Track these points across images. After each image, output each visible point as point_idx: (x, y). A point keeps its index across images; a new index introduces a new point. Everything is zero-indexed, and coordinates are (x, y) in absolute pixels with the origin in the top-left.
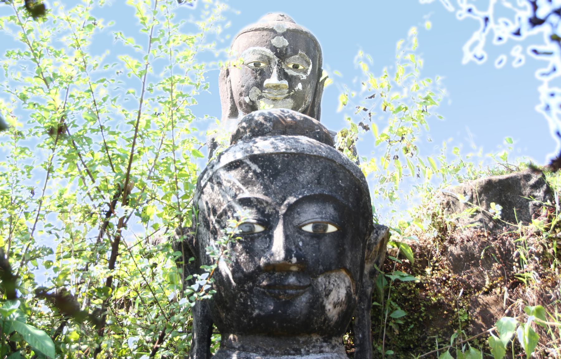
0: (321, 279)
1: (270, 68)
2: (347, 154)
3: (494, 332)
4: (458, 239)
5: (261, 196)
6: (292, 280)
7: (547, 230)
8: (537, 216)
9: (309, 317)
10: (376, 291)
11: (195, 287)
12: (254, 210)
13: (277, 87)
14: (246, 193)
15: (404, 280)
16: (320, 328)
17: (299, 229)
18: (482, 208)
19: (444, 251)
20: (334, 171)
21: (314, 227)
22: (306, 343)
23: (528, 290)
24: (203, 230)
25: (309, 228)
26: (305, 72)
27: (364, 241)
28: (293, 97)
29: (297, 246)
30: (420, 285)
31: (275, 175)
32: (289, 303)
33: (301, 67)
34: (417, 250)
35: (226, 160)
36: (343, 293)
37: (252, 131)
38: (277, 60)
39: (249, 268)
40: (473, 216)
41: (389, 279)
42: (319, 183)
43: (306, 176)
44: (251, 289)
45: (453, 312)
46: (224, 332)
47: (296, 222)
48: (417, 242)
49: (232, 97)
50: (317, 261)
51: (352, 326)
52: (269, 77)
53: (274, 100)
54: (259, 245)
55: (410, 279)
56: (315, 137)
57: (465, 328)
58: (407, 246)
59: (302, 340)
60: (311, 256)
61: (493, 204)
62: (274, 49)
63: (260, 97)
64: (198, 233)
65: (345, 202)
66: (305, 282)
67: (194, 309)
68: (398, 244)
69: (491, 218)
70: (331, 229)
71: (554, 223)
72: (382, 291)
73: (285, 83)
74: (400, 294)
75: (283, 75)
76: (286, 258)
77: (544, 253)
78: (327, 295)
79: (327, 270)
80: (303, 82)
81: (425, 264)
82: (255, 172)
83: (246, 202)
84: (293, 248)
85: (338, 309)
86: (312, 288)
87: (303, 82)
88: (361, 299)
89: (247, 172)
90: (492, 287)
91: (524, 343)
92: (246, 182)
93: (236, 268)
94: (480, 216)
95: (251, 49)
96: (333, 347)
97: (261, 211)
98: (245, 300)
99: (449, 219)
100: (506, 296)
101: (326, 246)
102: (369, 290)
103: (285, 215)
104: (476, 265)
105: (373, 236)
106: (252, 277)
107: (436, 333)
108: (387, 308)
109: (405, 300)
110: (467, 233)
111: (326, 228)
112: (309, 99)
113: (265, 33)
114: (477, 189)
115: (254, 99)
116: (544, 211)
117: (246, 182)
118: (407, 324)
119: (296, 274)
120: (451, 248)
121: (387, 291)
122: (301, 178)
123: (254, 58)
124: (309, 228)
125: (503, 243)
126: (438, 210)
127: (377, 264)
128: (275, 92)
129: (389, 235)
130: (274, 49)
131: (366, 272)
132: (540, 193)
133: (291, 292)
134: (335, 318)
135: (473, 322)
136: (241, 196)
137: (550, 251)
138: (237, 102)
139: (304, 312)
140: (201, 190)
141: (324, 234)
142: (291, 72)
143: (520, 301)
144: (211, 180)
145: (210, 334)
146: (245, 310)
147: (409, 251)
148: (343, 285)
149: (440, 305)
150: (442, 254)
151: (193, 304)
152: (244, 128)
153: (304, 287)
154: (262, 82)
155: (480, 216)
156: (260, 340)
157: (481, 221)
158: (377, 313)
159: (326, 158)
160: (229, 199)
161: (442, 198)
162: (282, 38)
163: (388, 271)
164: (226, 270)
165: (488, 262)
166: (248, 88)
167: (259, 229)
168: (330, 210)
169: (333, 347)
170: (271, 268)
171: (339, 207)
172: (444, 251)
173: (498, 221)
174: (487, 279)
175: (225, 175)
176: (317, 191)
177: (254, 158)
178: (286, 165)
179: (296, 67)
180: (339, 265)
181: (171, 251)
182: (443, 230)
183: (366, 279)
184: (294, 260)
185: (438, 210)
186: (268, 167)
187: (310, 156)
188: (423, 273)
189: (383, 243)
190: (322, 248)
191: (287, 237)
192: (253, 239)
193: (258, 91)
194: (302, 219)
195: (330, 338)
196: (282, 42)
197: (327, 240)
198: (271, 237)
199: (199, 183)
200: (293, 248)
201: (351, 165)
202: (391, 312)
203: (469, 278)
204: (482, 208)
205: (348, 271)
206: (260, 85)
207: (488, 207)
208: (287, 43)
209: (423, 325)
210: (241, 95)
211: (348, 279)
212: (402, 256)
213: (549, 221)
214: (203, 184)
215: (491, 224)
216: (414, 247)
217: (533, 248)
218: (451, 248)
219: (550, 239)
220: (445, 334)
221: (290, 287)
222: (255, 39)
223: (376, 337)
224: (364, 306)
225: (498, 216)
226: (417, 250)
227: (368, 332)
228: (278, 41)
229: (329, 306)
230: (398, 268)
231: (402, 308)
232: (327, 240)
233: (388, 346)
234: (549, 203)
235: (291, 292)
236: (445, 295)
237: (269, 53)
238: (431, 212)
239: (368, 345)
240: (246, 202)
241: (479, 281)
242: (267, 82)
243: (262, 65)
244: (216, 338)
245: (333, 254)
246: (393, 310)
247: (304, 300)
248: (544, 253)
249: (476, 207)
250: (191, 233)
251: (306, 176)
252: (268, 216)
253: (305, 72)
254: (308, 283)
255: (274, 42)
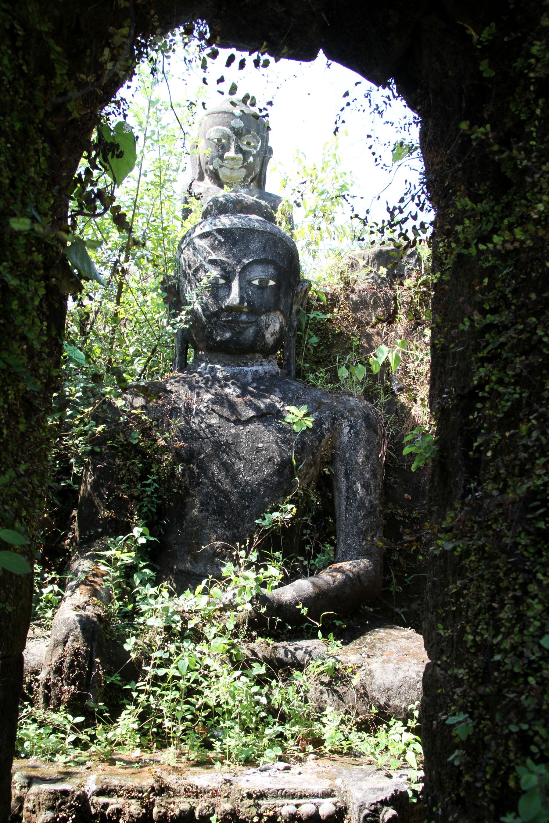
0: (263, 317)
1: (229, 144)
2: (283, 228)
3: (374, 355)
4: (357, 291)
5: (223, 259)
6: (244, 317)
7: (415, 286)
8: (410, 276)
9: (254, 342)
10: (300, 323)
11: (178, 319)
12: (219, 269)
13: (233, 159)
14: (214, 257)
15: (318, 317)
16: (261, 350)
17: (249, 282)
18: (374, 269)
19: (347, 298)
20: (275, 242)
21: (260, 282)
22: (251, 359)
23: (399, 326)
24: (182, 279)
25: (256, 282)
26: (255, 148)
27: (293, 291)
28: (245, 167)
29: (248, 294)
30: (329, 320)
31: (235, 243)
32: (241, 333)
33: (252, 144)
34: (329, 297)
35: (198, 231)
36: (277, 326)
37: (218, 209)
38: (234, 137)
39: (213, 308)
40: (368, 275)
41: (309, 317)
42: (264, 251)
43: (255, 245)
44: (215, 323)
45: (350, 339)
46: (196, 349)
47: (248, 278)
48: (328, 289)
49: (200, 164)
50: (261, 305)
51: (282, 347)
52: (228, 151)
53: (232, 169)
54: (221, 293)
55: (323, 317)
56: (262, 216)
57: (357, 351)
58: (321, 293)
59: (249, 357)
60: (257, 302)
61: (381, 268)
62: (232, 129)
63: (221, 166)
64: (179, 281)
65: (281, 264)
66: (252, 319)
67: (176, 334)
68: (316, 292)
69: (379, 277)
70: (272, 283)
71: (420, 282)
72: (304, 324)
73: (240, 156)
74: (316, 325)
75: (239, 150)
76: (240, 303)
77: (411, 301)
78: (267, 328)
79: (268, 311)
80: (254, 156)
81: (334, 306)
82: (219, 241)
83: (213, 262)
84: (245, 296)
85: (274, 337)
86: (257, 323)
87: (254, 156)
88: (289, 330)
89: (214, 241)
90: (376, 323)
91: (392, 361)
92: (213, 248)
93: (205, 308)
94: (372, 275)
95: (216, 128)
96: (269, 362)
97: (224, 269)
98: (212, 330)
99: (352, 276)
100: (385, 329)
101: (267, 294)
102: (295, 323)
103: (240, 272)
104: (367, 308)
105: (300, 287)
106: (216, 314)
107: (338, 352)
108: (307, 336)
109: (319, 330)
110: (363, 286)
111: (268, 282)
112: (258, 169)
113: (226, 115)
114: (372, 256)
115: (217, 167)
116: (414, 274)
117: (213, 248)
118: (319, 346)
119: (247, 313)
120: (352, 296)
121: (307, 324)
122: (251, 247)
123: (218, 135)
124: (256, 282)
125: (386, 294)
126: (345, 268)
127: (302, 305)
128: (232, 163)
129: (311, 286)
130: (232, 129)
131: (293, 311)
132: (413, 261)
133: (243, 325)
134: (272, 343)
135: (362, 346)
136: (210, 258)
137: (415, 301)
138: (204, 169)
139: (251, 339)
140: (181, 251)
141: (267, 287)
142: (245, 148)
143: (393, 334)
144: (188, 245)
145: (187, 348)
146: (210, 337)
147: (324, 298)
148: (278, 321)
149: (341, 334)
150: (346, 299)
151: (175, 331)
152: (211, 206)
153: (251, 323)
154: (223, 155)
155: (372, 275)
156: (220, 356)
157: (373, 278)
158: (299, 340)
159: (270, 233)
160: (200, 258)
161: (348, 260)
162: (238, 120)
163: (308, 310)
164: (197, 307)
165: (375, 306)
166: (212, 159)
167: (222, 281)
168: (271, 270)
169: (269, 362)
170: (230, 309)
171: (277, 268)
172: (347, 298)
173: (383, 279)
174: (374, 318)
175: (198, 242)
176: (263, 256)
177: (219, 231)
178: (242, 237)
179: (249, 144)
180: (276, 307)
181: (160, 291)
182: (347, 283)
183: (294, 316)
184: (246, 304)
185: (345, 268)
186: (229, 238)
187: (258, 231)
188: (332, 312)
189: (306, 292)
190: (265, 296)
191: (241, 288)
192: (217, 289)
193: (220, 161)
194: (252, 276)
195: (268, 355)
196: (239, 124)
197: (269, 290)
198: (230, 288)
199: (179, 246)
200: (245, 296)
201: (287, 237)
202: (309, 339)
203: (362, 316)
204: (374, 269)
205: (282, 312)
206: (221, 157)
207: (378, 269)
208: (243, 125)
209: (330, 347)
210: (207, 163)
211: (281, 317)
212: (319, 300)
213: (417, 280)
214: (183, 247)
215: (379, 281)
216: (327, 294)
217: (404, 299)
218: (352, 296)
219: (416, 293)
220: (343, 353)
221: (242, 322)
222: (218, 120)
223: (298, 355)
224: (291, 334)
225: (384, 275)
226: (329, 297)
227: (293, 352)
228: (236, 123)
229: (268, 336)
230: (316, 309)
231: (317, 335)
232: (269, 290)
233: (306, 361)
234: (418, 268)
235: (243, 325)
236: (346, 327)
237: (228, 131)
238: (340, 270)
239: (292, 360)
240: (213, 262)
241: (369, 319)
242: (226, 155)
243: (223, 141)
244: (191, 351)
245: (272, 300)
246: (310, 337)
247: (251, 332)
248: (411, 301)
249: (370, 269)
250: (174, 281)
251: (255, 245)
252: (229, 273)
253: (255, 148)
254: (254, 320)
255: (233, 123)
